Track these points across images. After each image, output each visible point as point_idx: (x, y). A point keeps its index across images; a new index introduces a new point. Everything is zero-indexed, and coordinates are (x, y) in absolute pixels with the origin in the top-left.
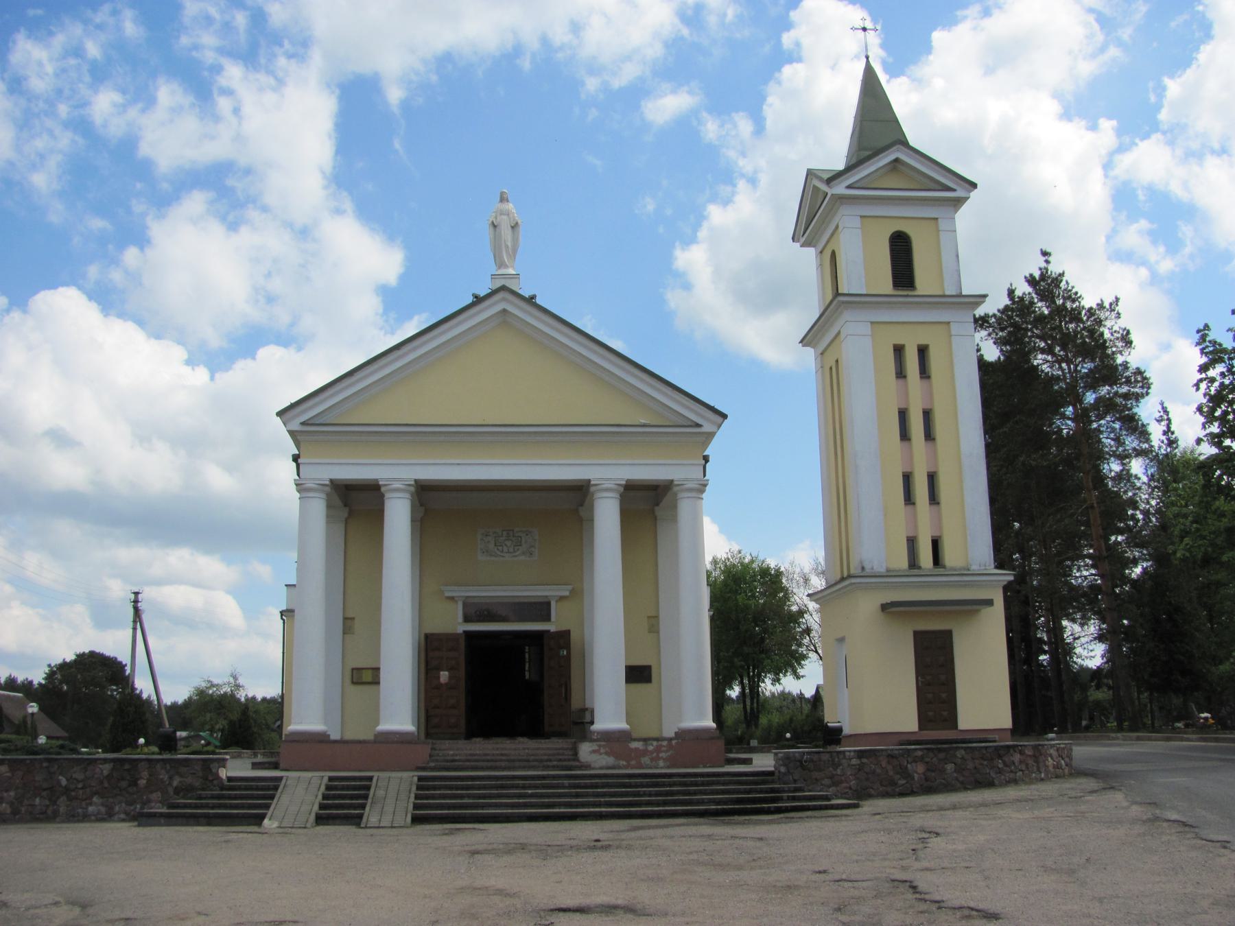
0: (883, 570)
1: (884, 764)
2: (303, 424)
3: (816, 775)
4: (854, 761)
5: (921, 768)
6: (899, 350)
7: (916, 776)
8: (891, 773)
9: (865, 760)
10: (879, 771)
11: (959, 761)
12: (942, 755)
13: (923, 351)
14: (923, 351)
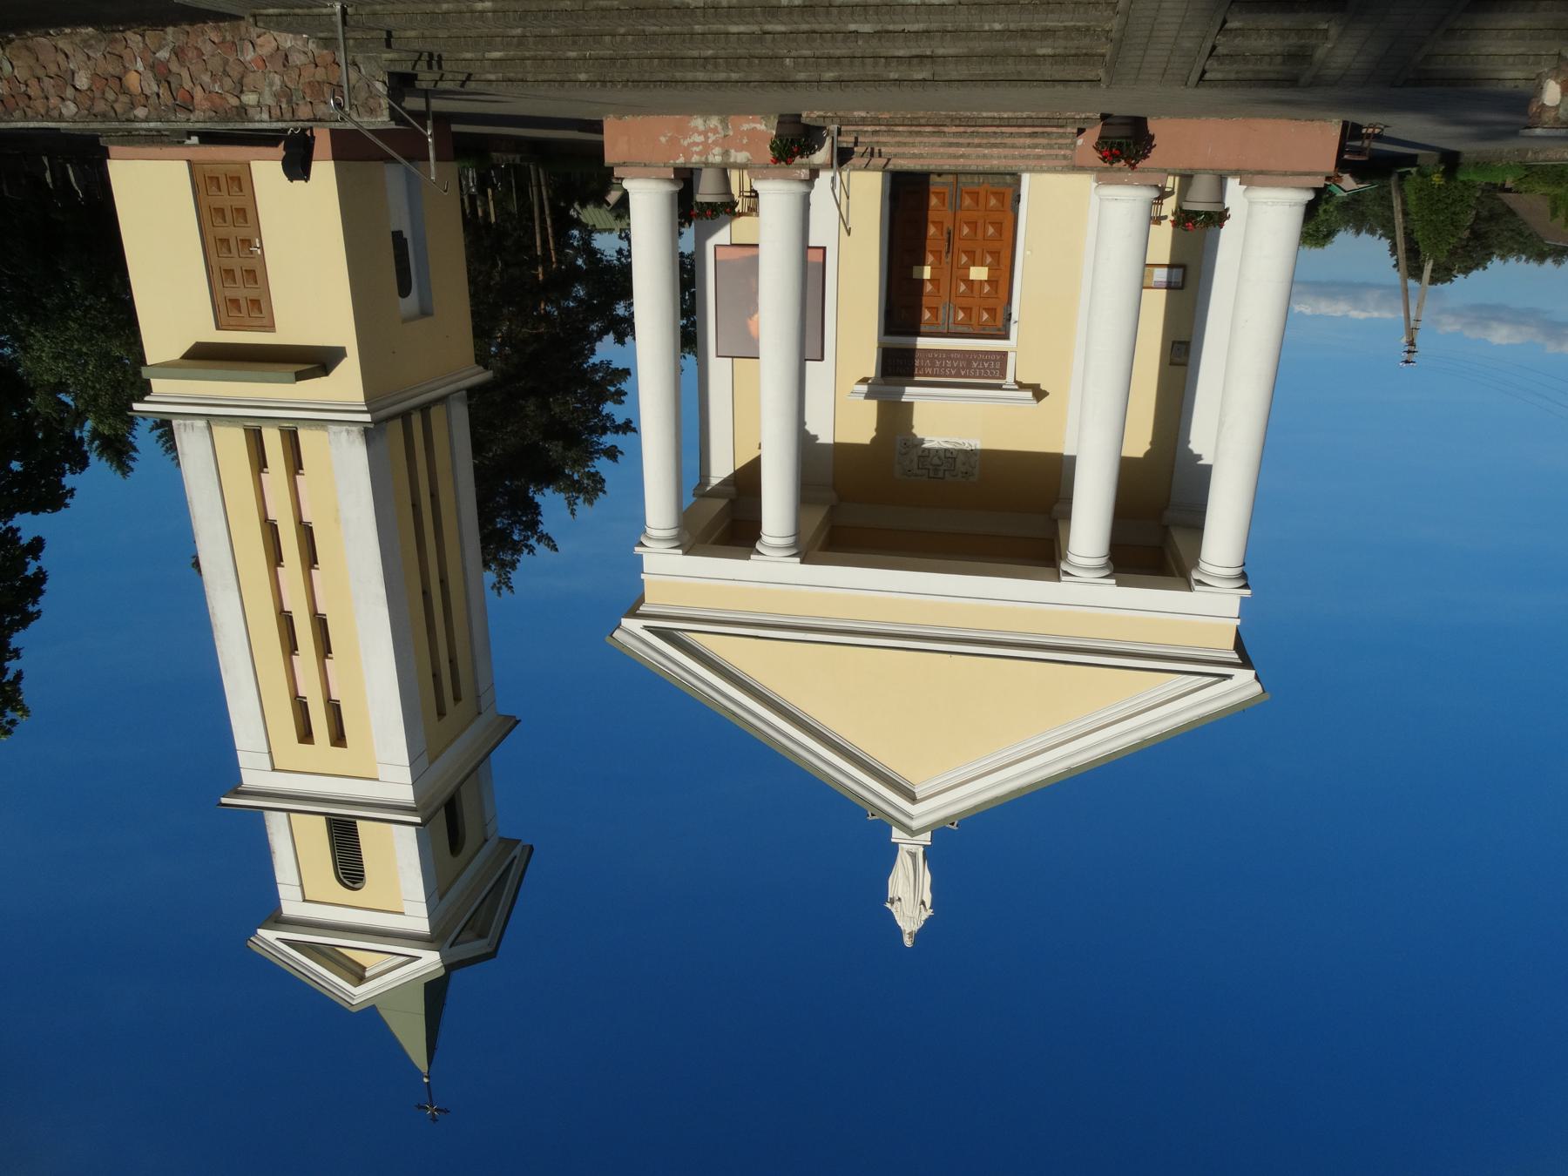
0: (333, 428)
1: (198, 94)
2: (1229, 677)
3: (320, 74)
4: (250, 99)
5: (132, 80)
6: (338, 738)
7: (140, 66)
8: (185, 74)
9: (234, 101)
10: (206, 78)
11: (70, 92)
12: (100, 106)
13: (306, 735)
14: (306, 735)
